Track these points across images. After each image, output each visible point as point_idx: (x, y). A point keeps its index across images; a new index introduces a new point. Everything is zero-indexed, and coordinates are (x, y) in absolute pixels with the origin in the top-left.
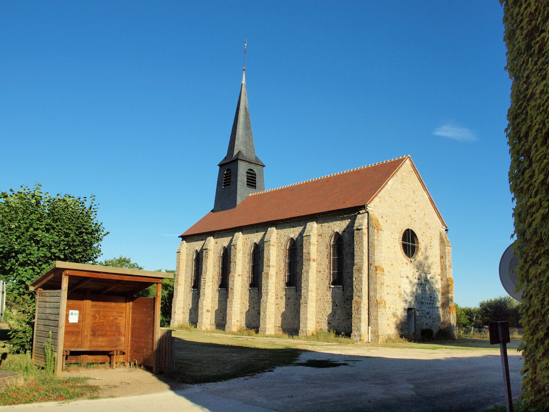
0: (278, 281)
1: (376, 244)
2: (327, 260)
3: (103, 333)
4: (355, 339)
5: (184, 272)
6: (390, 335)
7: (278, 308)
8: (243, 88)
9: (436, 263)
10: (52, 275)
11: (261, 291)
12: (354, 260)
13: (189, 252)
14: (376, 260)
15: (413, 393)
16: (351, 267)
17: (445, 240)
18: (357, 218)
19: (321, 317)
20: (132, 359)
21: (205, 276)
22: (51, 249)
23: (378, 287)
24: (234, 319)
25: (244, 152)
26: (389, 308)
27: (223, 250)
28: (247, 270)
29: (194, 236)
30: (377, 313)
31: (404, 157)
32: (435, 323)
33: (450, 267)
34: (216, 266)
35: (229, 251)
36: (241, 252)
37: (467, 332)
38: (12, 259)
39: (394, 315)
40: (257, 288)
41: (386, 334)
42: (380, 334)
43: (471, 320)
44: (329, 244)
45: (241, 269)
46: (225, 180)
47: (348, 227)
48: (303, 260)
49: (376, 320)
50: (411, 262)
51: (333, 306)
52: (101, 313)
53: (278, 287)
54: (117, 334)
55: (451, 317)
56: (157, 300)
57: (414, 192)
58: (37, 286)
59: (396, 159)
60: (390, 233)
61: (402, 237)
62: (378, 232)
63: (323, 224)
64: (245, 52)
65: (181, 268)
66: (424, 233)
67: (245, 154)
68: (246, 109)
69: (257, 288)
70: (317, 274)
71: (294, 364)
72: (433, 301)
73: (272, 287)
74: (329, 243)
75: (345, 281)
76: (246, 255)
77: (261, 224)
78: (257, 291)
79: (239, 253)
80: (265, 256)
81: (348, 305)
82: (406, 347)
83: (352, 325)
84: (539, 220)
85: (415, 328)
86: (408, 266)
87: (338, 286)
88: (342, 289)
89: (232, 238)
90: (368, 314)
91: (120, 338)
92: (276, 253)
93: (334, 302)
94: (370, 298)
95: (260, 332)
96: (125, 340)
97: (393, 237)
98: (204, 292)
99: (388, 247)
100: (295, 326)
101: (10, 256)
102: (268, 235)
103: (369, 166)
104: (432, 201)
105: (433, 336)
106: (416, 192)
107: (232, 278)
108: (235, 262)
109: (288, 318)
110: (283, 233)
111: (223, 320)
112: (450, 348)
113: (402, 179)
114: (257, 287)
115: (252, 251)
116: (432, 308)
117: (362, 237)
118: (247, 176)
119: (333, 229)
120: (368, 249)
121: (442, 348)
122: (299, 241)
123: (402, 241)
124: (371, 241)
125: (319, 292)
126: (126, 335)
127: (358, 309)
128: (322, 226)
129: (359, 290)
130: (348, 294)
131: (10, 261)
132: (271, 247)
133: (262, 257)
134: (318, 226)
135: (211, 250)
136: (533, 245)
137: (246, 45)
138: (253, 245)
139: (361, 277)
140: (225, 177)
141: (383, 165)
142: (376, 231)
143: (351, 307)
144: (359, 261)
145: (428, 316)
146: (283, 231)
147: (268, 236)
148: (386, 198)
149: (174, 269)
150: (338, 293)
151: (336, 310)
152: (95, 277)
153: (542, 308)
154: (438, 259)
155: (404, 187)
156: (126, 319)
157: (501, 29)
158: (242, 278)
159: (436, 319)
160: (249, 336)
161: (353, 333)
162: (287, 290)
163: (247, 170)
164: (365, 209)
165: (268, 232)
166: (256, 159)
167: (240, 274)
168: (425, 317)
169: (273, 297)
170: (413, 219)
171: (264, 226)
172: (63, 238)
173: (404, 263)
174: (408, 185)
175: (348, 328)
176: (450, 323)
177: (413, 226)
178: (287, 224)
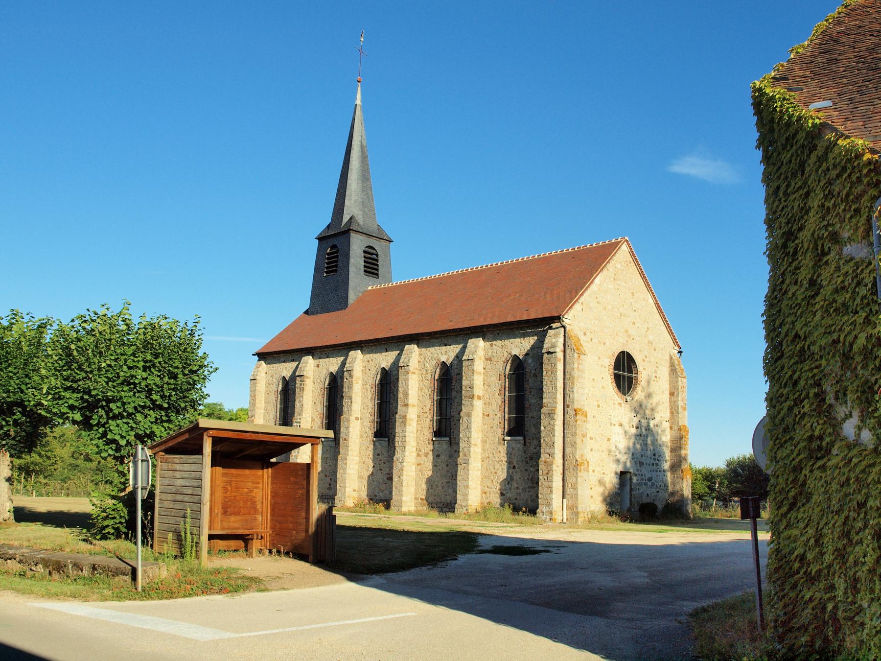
0: (420, 429)
1: (576, 375)
2: (500, 398)
3: (236, 510)
4: (544, 517)
5: (262, 411)
6: (594, 511)
7: (420, 471)
8: (358, 113)
9: (663, 403)
10: (187, 436)
11: (394, 443)
12: (542, 398)
13: (271, 379)
14: (575, 399)
15: (647, 580)
16: (537, 409)
17: (677, 367)
18: (548, 335)
19: (489, 484)
20: (273, 545)
21: (300, 419)
22: (151, 394)
23: (578, 440)
25: (360, 218)
26: (594, 471)
27: (328, 378)
28: (370, 409)
29: (279, 354)
30: (577, 479)
31: (619, 240)
32: (660, 495)
33: (684, 409)
34: (318, 402)
35: (339, 380)
36: (360, 382)
37: (706, 507)
38: (100, 409)
39: (601, 482)
40: (387, 439)
41: (588, 510)
42: (579, 510)
43: (711, 488)
44: (502, 374)
45: (360, 408)
46: (327, 263)
47: (533, 348)
48: (462, 397)
49: (575, 489)
50: (627, 401)
51: (508, 468)
52: (234, 484)
53: (421, 438)
54: (252, 511)
55: (684, 485)
56: (313, 467)
57: (633, 294)
58: (157, 449)
59: (607, 242)
61: (613, 364)
62: (579, 356)
63: (494, 343)
64: (361, 52)
65: (258, 405)
66: (646, 357)
67: (361, 223)
68: (362, 147)
69: (387, 439)
70: (483, 418)
71: (477, 550)
72: (658, 460)
73: (411, 438)
74: (503, 371)
75: (527, 431)
76: (369, 387)
77: (393, 338)
78: (386, 444)
80: (400, 389)
81: (532, 466)
82: (620, 530)
83: (537, 496)
84: (786, 410)
87: (517, 438)
88: (523, 442)
89: (346, 359)
90: (563, 480)
91: (256, 517)
93: (509, 462)
94: (565, 456)
95: (392, 507)
96: (262, 520)
99: (593, 380)
100: (449, 499)
101: (99, 405)
102: (405, 356)
103: (565, 251)
104: (659, 307)
105: (657, 513)
106: (635, 294)
107: (346, 423)
108: (350, 398)
109: (436, 485)
110: (429, 354)
111: (330, 489)
112: (684, 531)
113: (615, 275)
114: (385, 437)
115: (377, 381)
116: (657, 471)
117: (555, 364)
118: (364, 257)
119: (509, 351)
120: (564, 383)
121: (673, 530)
122: (455, 367)
123: (614, 370)
124: (569, 370)
125: (487, 446)
126: (264, 513)
128: (491, 345)
129: (549, 445)
130: (532, 449)
131: (97, 412)
132: (410, 375)
133: (395, 390)
134: (485, 344)
136: (781, 430)
137: (362, 39)
138: (380, 371)
139: (554, 425)
140: (328, 259)
141: (587, 251)
142: (576, 355)
143: (538, 470)
145: (649, 483)
146: (429, 351)
147: (406, 358)
149: (246, 406)
150: (516, 449)
151: (513, 473)
152: (242, 438)
153: (786, 486)
156: (263, 491)
157: (761, 212)
158: (362, 423)
159: (661, 488)
160: (375, 513)
161: (540, 508)
162: (436, 442)
163: (364, 248)
164: (560, 322)
165: (404, 352)
166: (379, 229)
167: (359, 416)
168: (646, 484)
169: (412, 454)
171: (399, 342)
172: (166, 379)
173: (617, 403)
174: (623, 284)
175: (532, 501)
176: (683, 494)
178: (436, 340)
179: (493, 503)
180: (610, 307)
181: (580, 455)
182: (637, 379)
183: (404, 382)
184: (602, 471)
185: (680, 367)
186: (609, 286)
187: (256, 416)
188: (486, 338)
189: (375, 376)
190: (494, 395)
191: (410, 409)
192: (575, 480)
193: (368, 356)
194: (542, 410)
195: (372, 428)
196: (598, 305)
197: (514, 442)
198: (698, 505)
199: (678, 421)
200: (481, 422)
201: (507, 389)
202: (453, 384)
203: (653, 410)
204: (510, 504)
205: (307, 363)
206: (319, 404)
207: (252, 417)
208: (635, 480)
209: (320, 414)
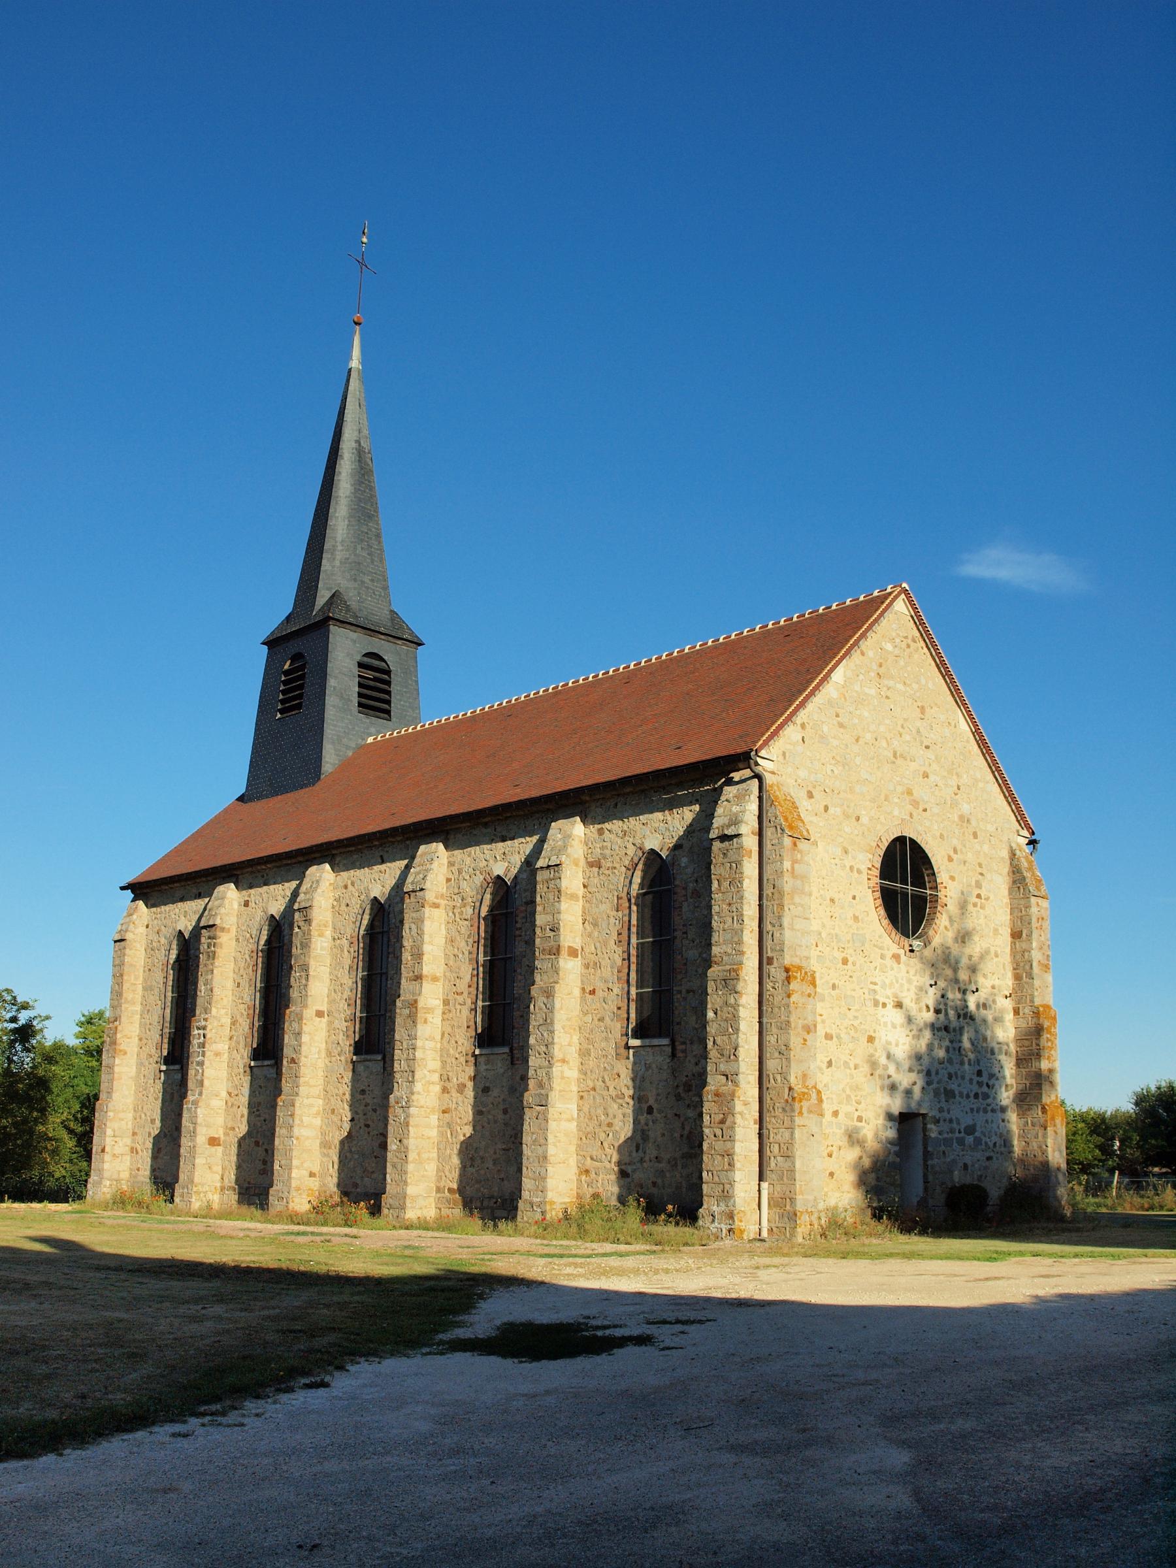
0: (449, 1030)
1: (787, 888)
2: (619, 950)
4: (713, 1228)
5: (138, 1008)
8: (354, 384)
9: (997, 956)
12: (710, 945)
13: (156, 938)
15: (903, 1499)
17: (1027, 875)
18: (723, 798)
21: (205, 1020)
23: (795, 1041)
24: (297, 1167)
25: (352, 597)
26: (836, 1114)
28: (347, 994)
30: (792, 1134)
31: (889, 590)
33: (1046, 968)
34: (245, 983)
36: (328, 933)
37: (1098, 1188)
40: (379, 1057)
41: (821, 1206)
43: (1106, 1149)
44: (624, 895)
46: (284, 692)
49: (788, 1157)
50: (912, 951)
51: (637, 1113)
53: (452, 1052)
55: (1050, 1142)
60: (839, 851)
61: (878, 865)
62: (795, 844)
63: (607, 826)
64: (362, 264)
65: (128, 995)
66: (955, 851)
67: (353, 604)
68: (360, 452)
69: (379, 1057)
70: (583, 999)
72: (988, 1086)
73: (428, 1052)
74: (626, 889)
76: (345, 943)
78: (378, 1067)
80: (405, 943)
86: (902, 966)
87: (656, 1042)
88: (669, 1049)
90: (760, 1135)
95: (385, 1211)
98: (199, 1078)
99: (832, 900)
102: (418, 869)
105: (989, 1208)
106: (928, 710)
107: (295, 1025)
108: (305, 968)
109: (482, 1158)
110: (468, 860)
112: (1050, 1255)
113: (881, 666)
115: (363, 928)
116: (985, 1111)
117: (738, 863)
119: (638, 842)
120: (760, 906)
121: (1021, 1254)
127: (723, 1122)
129: (726, 1053)
132: (427, 911)
135: (229, 931)
137: (365, 240)
138: (369, 907)
139: (736, 1007)
142: (787, 841)
144: (729, 951)
145: (970, 1139)
151: (647, 1124)
155: (889, 694)
158: (330, 1023)
161: (705, 1206)
163: (358, 658)
165: (417, 861)
166: (392, 620)
167: (324, 1008)
168: (961, 1142)
169: (432, 1087)
173: (889, 954)
174: (900, 686)
178: (484, 831)
179: (604, 1196)
180: (868, 736)
181: (800, 1073)
182: (935, 899)
183: (413, 926)
184: (857, 1114)
185: (1033, 874)
186: (867, 690)
187: (123, 1019)
188: (589, 816)
189: (360, 917)
190: (605, 944)
191: (427, 987)
192: (787, 1134)
193: (344, 874)
194: (710, 972)
195: (351, 1033)
196: (842, 730)
197: (649, 1049)
198: (1080, 1184)
199: (1032, 996)
200: (576, 1011)
201: (634, 929)
202: (518, 925)
203: (973, 970)
204: (641, 1196)
205: (223, 898)
206: (247, 985)
207: (116, 1021)
208: (933, 1131)
209: (249, 1008)
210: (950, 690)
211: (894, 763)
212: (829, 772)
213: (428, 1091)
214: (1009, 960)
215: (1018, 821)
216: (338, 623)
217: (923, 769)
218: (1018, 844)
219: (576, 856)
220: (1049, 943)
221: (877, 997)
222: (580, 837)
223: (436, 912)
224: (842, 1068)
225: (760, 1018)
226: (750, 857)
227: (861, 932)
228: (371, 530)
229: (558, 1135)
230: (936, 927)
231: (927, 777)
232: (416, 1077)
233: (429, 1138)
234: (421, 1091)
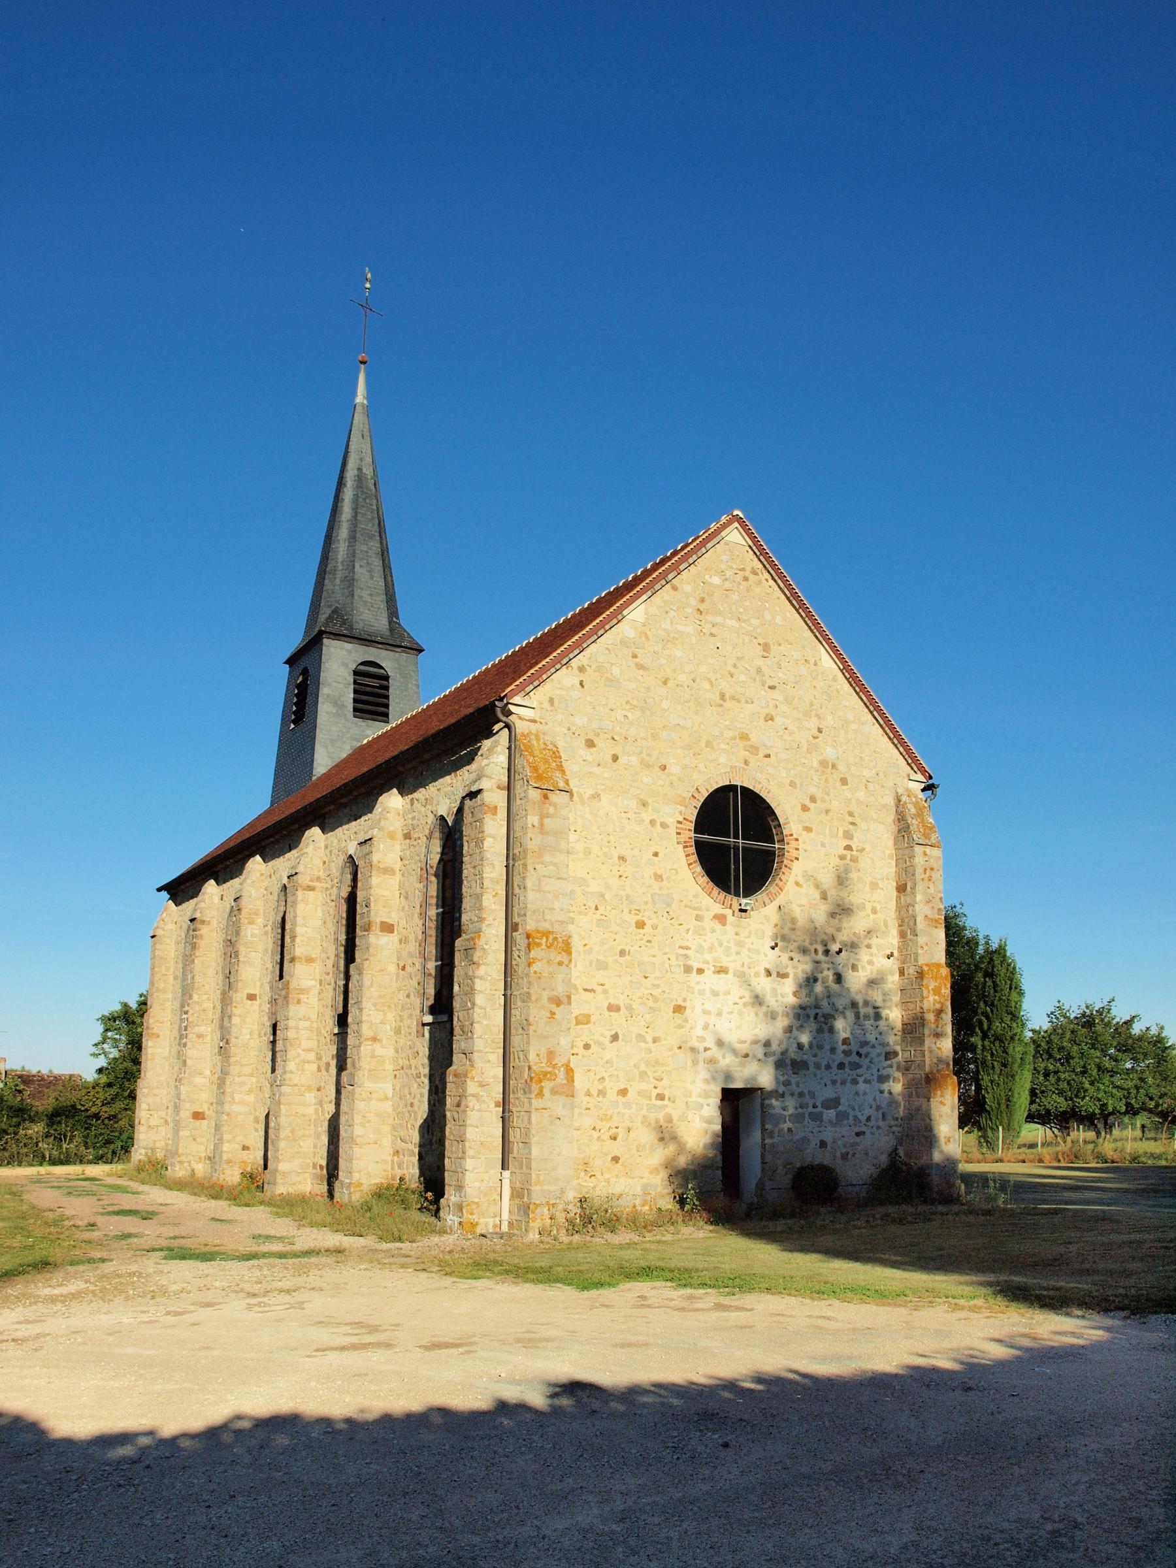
24: (228, 1141)
30: (530, 1116)
57: (766, 647)
60: (633, 804)
61: (693, 818)
62: (546, 797)
66: (813, 799)
73: (303, 1032)
76: (269, 928)
79: (249, 923)
85: (763, 1163)
86: (728, 927)
92: (320, 914)
97: (647, 816)
106: (774, 648)
123: (695, 833)
127: (458, 1105)
135: (209, 923)
137: (368, 285)
145: (830, 1114)
148: (616, 671)
154: (889, 889)
155: (714, 631)
159: (873, 1123)
170: (757, 749)
174: (734, 623)
177: (759, 776)
181: (544, 1052)
186: (680, 628)
196: (641, 672)
199: (916, 954)
210: (807, 624)
211: (721, 705)
212: (622, 719)
213: (303, 1070)
214: (894, 917)
215: (908, 764)
216: (332, 636)
217: (765, 711)
218: (908, 791)
219: (391, 829)
220: (942, 895)
221: (689, 963)
222: (397, 809)
223: (311, 894)
224: (634, 1041)
225: (505, 990)
226: (495, 813)
227: (665, 891)
228: (371, 549)
229: (367, 1115)
230: (780, 884)
231: (772, 719)
232: (288, 1056)
233: (304, 1115)
234: (294, 1069)
